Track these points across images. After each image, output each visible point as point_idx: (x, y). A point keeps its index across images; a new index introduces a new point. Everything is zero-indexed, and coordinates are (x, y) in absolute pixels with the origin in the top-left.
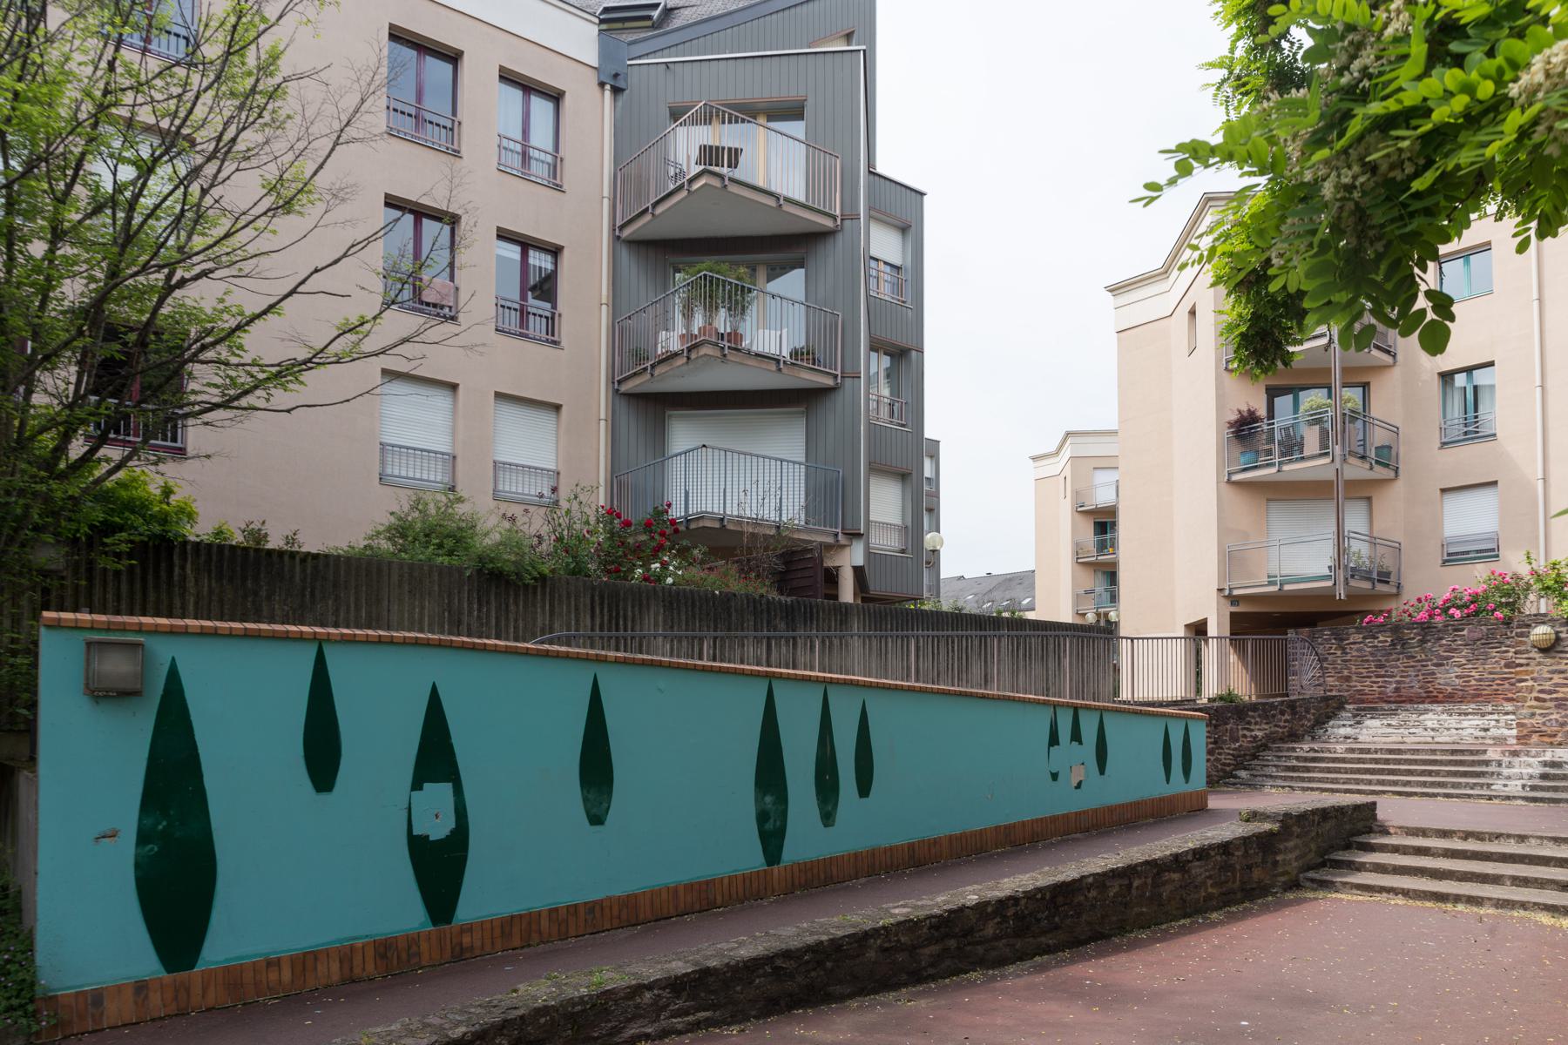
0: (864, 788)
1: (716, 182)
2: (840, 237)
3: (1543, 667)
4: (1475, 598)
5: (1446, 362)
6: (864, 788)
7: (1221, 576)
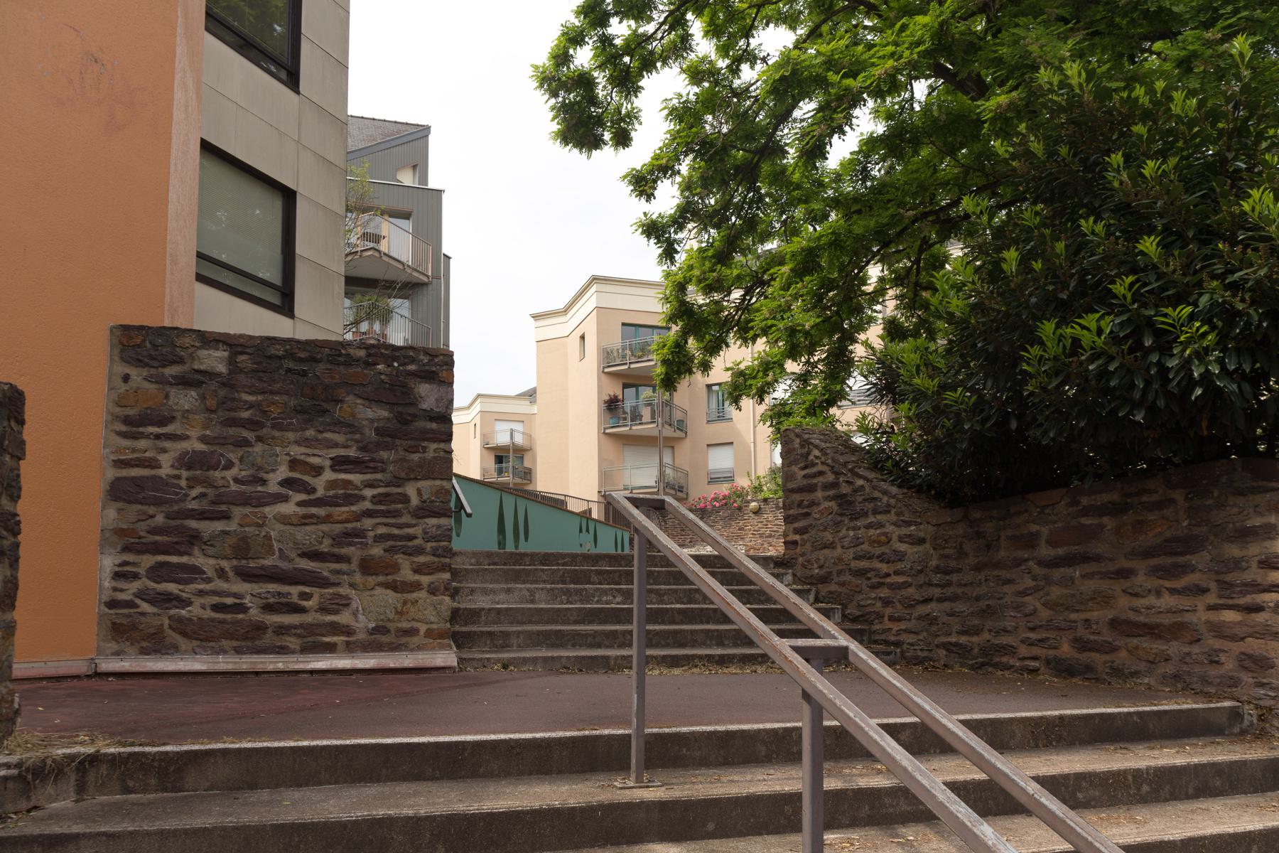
0: (526, 540)
1: (377, 254)
2: (430, 287)
3: (754, 520)
4: (725, 497)
5: (710, 380)
6: (526, 540)
7: (600, 485)
